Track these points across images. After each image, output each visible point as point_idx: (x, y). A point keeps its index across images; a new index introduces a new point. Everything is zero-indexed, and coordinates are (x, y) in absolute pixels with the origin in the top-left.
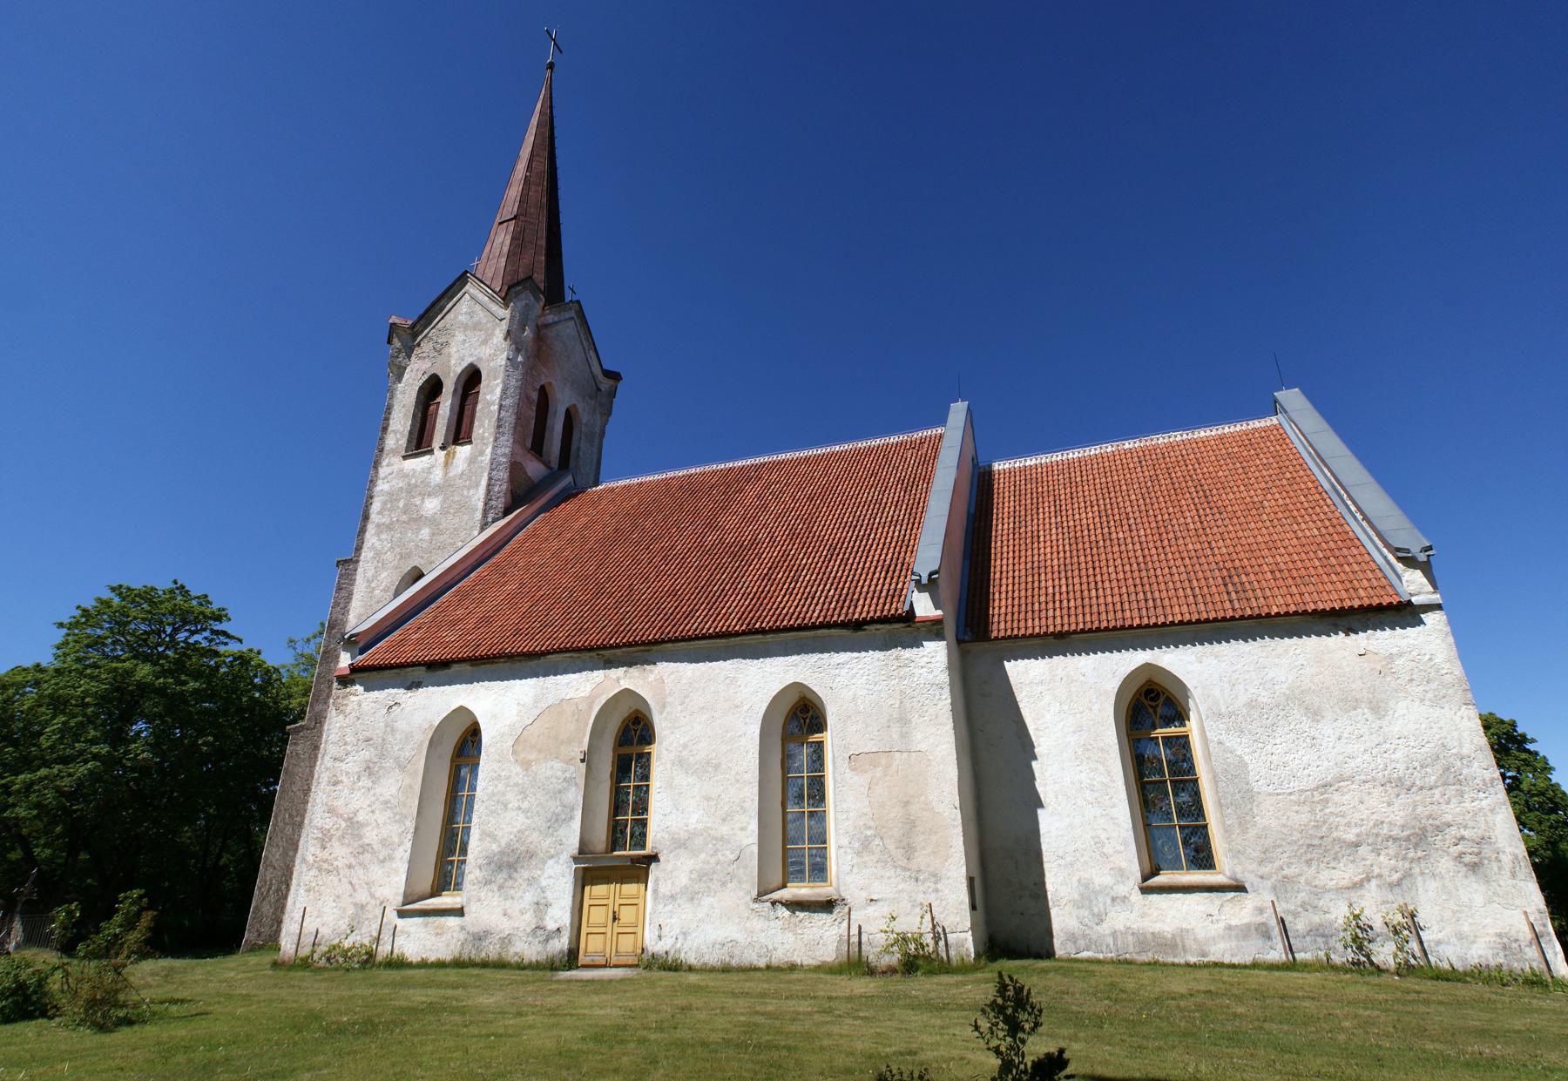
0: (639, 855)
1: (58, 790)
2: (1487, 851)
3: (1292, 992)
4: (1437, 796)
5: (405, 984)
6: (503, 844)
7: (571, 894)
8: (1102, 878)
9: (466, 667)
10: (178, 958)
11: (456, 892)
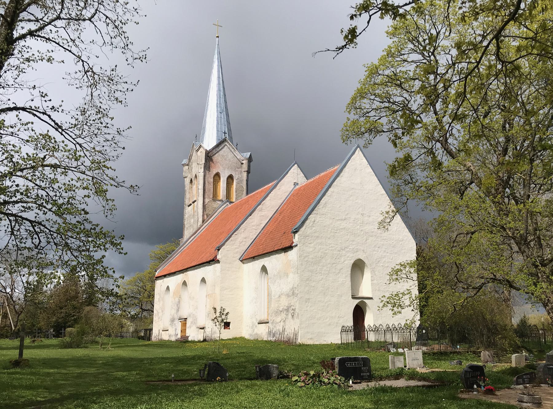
0: (279, 212)
1: (507, 16)
3: (198, 382)
4: (85, 184)
5: (343, 338)
6: (212, 385)
7: (132, 357)
9: (251, 259)
10: (204, 128)
11: (329, 356)
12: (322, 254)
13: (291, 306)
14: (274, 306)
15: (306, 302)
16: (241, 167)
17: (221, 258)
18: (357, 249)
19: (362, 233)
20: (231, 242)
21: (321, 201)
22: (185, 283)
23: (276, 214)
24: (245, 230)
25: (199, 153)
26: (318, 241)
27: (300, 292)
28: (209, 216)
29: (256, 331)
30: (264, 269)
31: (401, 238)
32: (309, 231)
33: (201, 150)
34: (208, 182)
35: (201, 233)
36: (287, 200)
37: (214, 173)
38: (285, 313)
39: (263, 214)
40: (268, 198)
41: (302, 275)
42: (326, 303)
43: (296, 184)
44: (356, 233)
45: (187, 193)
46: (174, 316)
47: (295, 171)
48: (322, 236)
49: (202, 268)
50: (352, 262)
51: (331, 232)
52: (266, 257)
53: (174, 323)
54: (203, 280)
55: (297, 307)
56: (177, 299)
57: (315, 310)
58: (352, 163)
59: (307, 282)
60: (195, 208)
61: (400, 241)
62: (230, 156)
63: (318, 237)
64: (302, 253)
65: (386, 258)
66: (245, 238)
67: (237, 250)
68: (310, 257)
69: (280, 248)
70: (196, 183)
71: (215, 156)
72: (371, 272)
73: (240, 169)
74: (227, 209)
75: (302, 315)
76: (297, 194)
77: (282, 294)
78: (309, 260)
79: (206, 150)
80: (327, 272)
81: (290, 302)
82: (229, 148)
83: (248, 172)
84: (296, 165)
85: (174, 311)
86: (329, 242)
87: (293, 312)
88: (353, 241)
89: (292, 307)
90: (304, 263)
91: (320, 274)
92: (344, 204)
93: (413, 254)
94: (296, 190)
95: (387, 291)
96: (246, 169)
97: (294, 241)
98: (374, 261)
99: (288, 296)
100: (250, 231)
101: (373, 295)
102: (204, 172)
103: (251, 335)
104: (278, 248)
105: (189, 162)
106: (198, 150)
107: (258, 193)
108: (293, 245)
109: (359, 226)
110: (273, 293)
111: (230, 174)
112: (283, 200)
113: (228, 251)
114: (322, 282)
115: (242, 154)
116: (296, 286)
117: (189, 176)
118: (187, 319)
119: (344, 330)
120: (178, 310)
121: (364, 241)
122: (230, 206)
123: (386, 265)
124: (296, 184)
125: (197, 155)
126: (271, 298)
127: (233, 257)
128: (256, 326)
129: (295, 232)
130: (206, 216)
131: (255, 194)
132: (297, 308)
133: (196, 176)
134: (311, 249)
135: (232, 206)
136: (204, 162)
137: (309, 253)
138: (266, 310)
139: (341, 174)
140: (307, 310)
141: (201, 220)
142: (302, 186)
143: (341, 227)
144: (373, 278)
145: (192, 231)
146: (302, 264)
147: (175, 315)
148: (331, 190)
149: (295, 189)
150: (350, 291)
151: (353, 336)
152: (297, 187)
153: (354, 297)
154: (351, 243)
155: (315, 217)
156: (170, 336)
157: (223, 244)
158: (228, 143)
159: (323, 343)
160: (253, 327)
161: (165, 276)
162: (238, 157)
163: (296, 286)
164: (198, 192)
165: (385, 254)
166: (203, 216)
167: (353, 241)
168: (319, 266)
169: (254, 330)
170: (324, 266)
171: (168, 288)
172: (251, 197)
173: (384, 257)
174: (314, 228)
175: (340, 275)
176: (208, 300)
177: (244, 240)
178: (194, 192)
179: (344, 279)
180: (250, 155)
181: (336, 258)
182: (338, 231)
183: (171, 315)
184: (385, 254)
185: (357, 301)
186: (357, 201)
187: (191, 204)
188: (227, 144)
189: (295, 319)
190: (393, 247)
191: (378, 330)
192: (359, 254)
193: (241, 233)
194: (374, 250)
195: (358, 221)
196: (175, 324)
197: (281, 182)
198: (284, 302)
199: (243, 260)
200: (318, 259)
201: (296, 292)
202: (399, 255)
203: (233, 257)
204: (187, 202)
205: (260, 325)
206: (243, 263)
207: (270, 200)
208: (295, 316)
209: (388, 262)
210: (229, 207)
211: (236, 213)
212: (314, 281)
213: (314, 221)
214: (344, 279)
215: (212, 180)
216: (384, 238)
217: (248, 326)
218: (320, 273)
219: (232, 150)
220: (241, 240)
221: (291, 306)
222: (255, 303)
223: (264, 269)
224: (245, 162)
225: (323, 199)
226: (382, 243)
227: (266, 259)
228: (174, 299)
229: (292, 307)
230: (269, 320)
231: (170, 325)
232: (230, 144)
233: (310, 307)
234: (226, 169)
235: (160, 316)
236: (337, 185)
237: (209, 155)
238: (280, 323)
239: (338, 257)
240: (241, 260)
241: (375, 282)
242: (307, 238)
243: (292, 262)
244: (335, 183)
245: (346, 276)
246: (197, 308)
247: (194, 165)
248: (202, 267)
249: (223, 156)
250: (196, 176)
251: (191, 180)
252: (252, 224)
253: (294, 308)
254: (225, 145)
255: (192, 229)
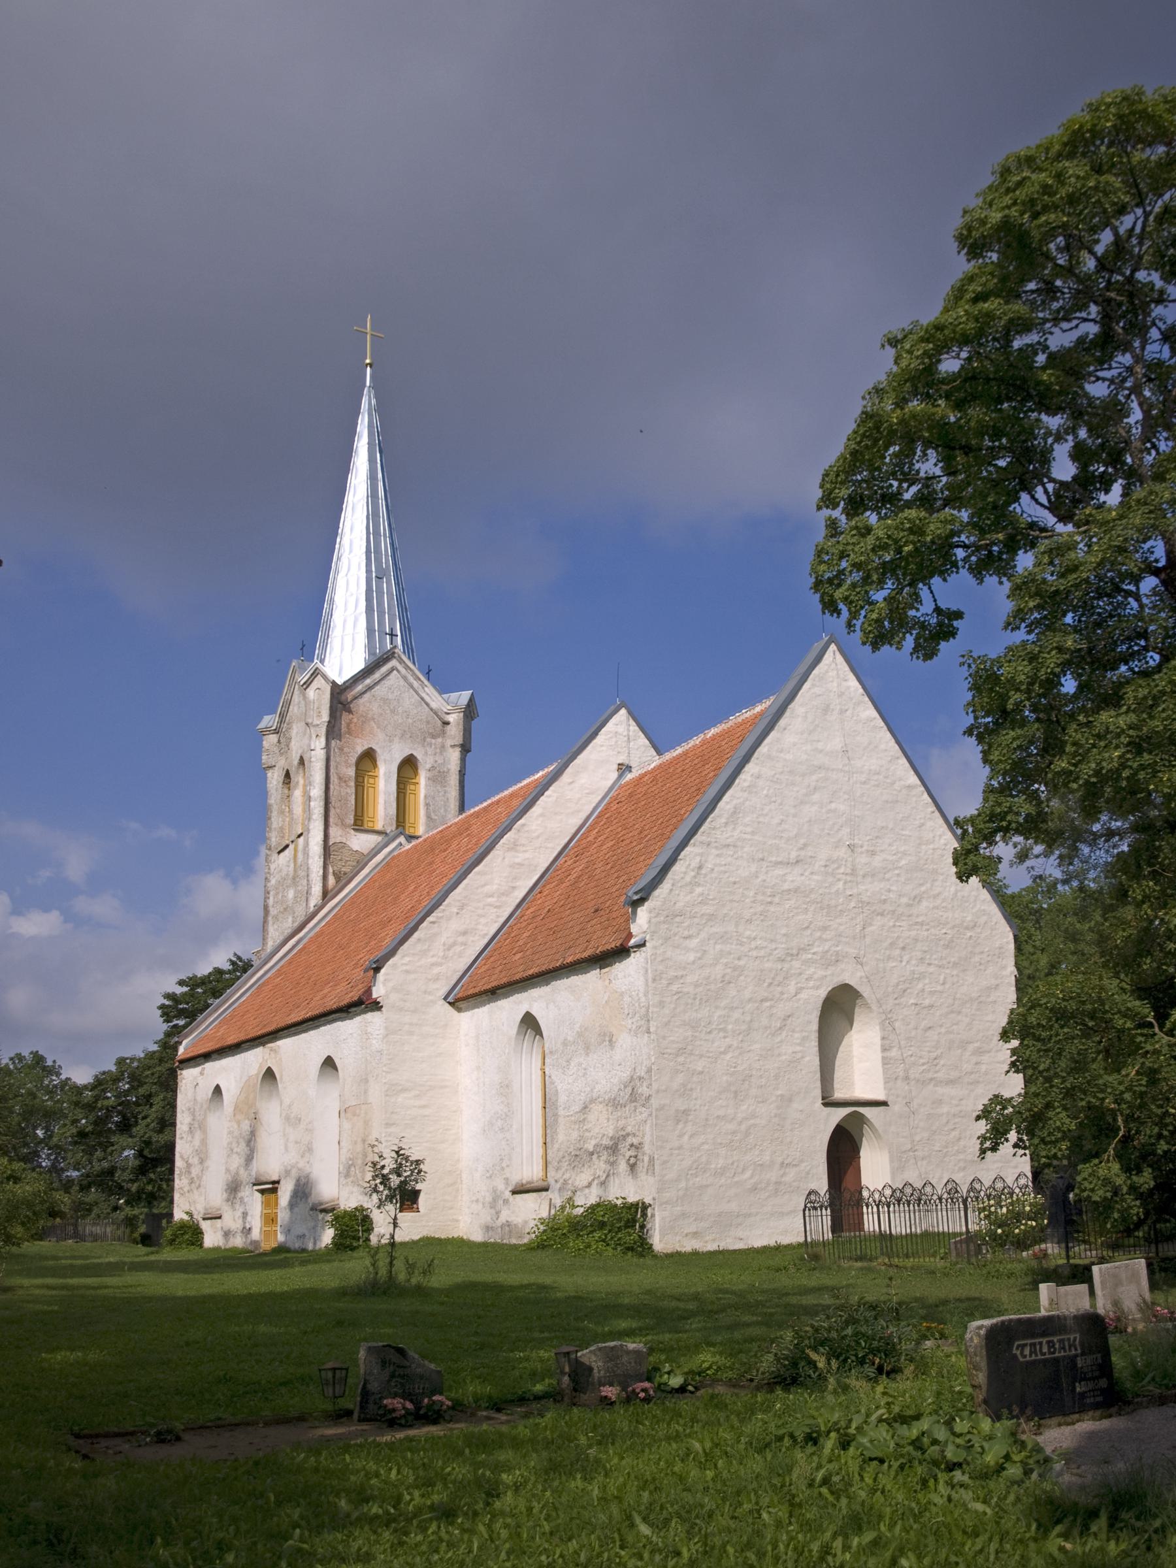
2: (640, 1157)
8: (501, 1186)
9: (484, 998)
12: (729, 971)
13: (625, 1137)
14: (564, 1136)
15: (678, 1121)
16: (444, 732)
17: (387, 995)
18: (837, 953)
19: (853, 904)
20: (419, 947)
21: (721, 804)
22: (269, 1075)
23: (561, 860)
24: (462, 908)
25: (311, 693)
26: (714, 930)
27: (658, 1091)
28: (343, 879)
29: (505, 1216)
30: (530, 1023)
31: (969, 918)
32: (683, 899)
33: (318, 682)
34: (340, 778)
35: (317, 929)
36: (598, 817)
37: (360, 750)
38: (604, 1158)
39: (520, 857)
40: (536, 810)
41: (664, 1038)
42: (740, 1123)
43: (624, 768)
44: (833, 903)
45: (274, 814)
46: (237, 1173)
47: (621, 729)
48: (726, 915)
49: (323, 1028)
50: (823, 993)
51: (754, 902)
52: (534, 986)
53: (240, 1195)
54: (329, 1063)
55: (648, 1137)
56: (246, 1126)
57: (706, 1147)
58: (817, 690)
59: (681, 1059)
60: (300, 856)
61: (967, 928)
62: (409, 700)
63: (711, 917)
64: (661, 967)
65: (927, 981)
66: (465, 933)
67: (436, 970)
68: (689, 979)
69: (586, 954)
70: (301, 782)
71: (361, 701)
72: (882, 1024)
73: (440, 740)
74: (399, 855)
75: (665, 1162)
76: (631, 795)
77: (592, 1101)
78: (685, 990)
79: (334, 683)
80: (744, 1027)
81: (621, 1123)
82: (405, 678)
83: (465, 748)
84: (623, 711)
85: (237, 1162)
86: (748, 933)
87: (632, 1153)
88: (825, 928)
89: (630, 1140)
90: (668, 1000)
91: (721, 1034)
92: (795, 816)
93: (1004, 968)
94: (627, 784)
95: (931, 1079)
96: (459, 740)
97: (634, 929)
98: (890, 989)
99: (614, 1104)
100: (480, 912)
101: (887, 1095)
102: (328, 746)
103: (488, 1228)
104: (578, 957)
105: (281, 722)
106: (308, 684)
107: (498, 802)
108: (632, 942)
109: (841, 883)
110: (562, 1098)
111: (407, 753)
112: (584, 815)
113: (407, 972)
114: (728, 1057)
115: (445, 696)
116: (641, 1072)
117: (282, 763)
118: (278, 1182)
119: (811, 1204)
120: (249, 1159)
121: (859, 928)
122: (408, 846)
123: (927, 1002)
124: (624, 768)
125: (305, 697)
126: (556, 1115)
127: (425, 992)
128: (506, 1201)
129: (637, 903)
130: (331, 880)
131: (489, 806)
132: (647, 1139)
133: (302, 761)
134: (691, 957)
135: (415, 847)
136: (325, 717)
137: (685, 968)
138: (538, 1151)
139: (782, 722)
140: (680, 1148)
141: (317, 889)
142: (645, 774)
143: (786, 886)
144: (887, 1042)
145: (289, 924)
146: (661, 1004)
147: (242, 1171)
148: (751, 768)
149: (623, 782)
150: (818, 1084)
151: (828, 1221)
152: (629, 777)
153: (829, 1103)
154: (818, 934)
155: (701, 855)
156: (227, 1234)
157: (392, 953)
158: (401, 661)
159: (731, 1248)
160: (495, 1202)
161: (207, 1056)
162: (434, 705)
163: (641, 1072)
164: (307, 809)
165: (922, 968)
166: (325, 877)
167: (825, 928)
168: (717, 1007)
169: (498, 1213)
170: (732, 1009)
171: (218, 1090)
172: (477, 815)
173: (919, 979)
174: (699, 890)
175: (784, 1034)
176: (347, 1125)
177: (461, 939)
178: (298, 809)
179: (798, 1048)
180: (471, 700)
181: (770, 984)
182: (776, 900)
183: (228, 1170)
184: (922, 968)
185: (843, 1112)
186: (833, 806)
187: (287, 846)
188: (400, 667)
189: (642, 1176)
190: (947, 946)
191: (920, 1200)
192: (843, 970)
193: (449, 919)
194: (889, 958)
195: (838, 868)
196: (242, 1198)
197: (577, 761)
198: (602, 1125)
199: (457, 1000)
200: (713, 987)
201: (643, 1090)
202: (964, 971)
203: (425, 992)
204: (274, 839)
205: (518, 1197)
206: (459, 1010)
207: (542, 815)
208: (642, 1166)
209: (932, 993)
210: (408, 851)
211: (431, 863)
212: (701, 1056)
213: (700, 868)
214: (798, 1048)
215: (351, 772)
216: (920, 920)
217: (477, 1201)
218: (721, 1030)
219: (416, 684)
220: (451, 940)
221: (625, 1137)
222: (502, 1129)
223: (530, 1023)
224: (454, 718)
225: (726, 798)
226: (913, 933)
227: (535, 992)
228: (239, 1123)
229: (630, 1140)
230: (551, 1181)
231: (228, 1200)
232: (407, 667)
233: (691, 1136)
234: (396, 739)
235: (194, 1174)
236: (769, 757)
237: (343, 698)
238: (587, 1191)
239: (779, 978)
240: (450, 999)
241: (894, 1053)
242: (678, 919)
243: (627, 999)
244: (763, 749)
245: (804, 1039)
246: (309, 1149)
247: (296, 730)
248: (324, 1025)
249: (385, 700)
250: (302, 761)
251: (287, 775)
252: (487, 889)
253: (635, 1141)
254: (393, 669)
255: (290, 919)
